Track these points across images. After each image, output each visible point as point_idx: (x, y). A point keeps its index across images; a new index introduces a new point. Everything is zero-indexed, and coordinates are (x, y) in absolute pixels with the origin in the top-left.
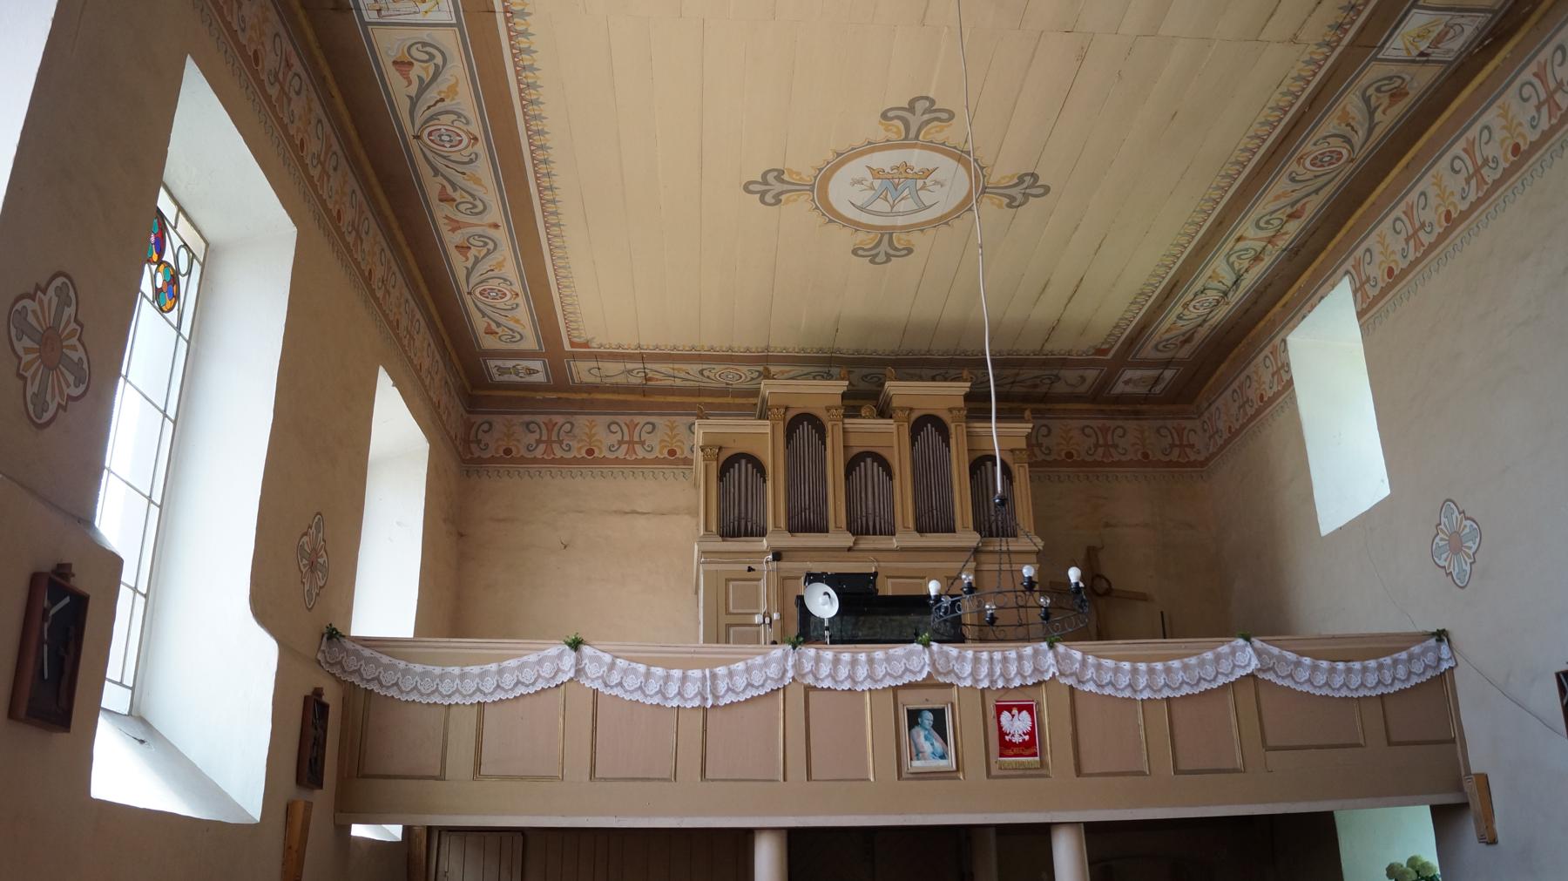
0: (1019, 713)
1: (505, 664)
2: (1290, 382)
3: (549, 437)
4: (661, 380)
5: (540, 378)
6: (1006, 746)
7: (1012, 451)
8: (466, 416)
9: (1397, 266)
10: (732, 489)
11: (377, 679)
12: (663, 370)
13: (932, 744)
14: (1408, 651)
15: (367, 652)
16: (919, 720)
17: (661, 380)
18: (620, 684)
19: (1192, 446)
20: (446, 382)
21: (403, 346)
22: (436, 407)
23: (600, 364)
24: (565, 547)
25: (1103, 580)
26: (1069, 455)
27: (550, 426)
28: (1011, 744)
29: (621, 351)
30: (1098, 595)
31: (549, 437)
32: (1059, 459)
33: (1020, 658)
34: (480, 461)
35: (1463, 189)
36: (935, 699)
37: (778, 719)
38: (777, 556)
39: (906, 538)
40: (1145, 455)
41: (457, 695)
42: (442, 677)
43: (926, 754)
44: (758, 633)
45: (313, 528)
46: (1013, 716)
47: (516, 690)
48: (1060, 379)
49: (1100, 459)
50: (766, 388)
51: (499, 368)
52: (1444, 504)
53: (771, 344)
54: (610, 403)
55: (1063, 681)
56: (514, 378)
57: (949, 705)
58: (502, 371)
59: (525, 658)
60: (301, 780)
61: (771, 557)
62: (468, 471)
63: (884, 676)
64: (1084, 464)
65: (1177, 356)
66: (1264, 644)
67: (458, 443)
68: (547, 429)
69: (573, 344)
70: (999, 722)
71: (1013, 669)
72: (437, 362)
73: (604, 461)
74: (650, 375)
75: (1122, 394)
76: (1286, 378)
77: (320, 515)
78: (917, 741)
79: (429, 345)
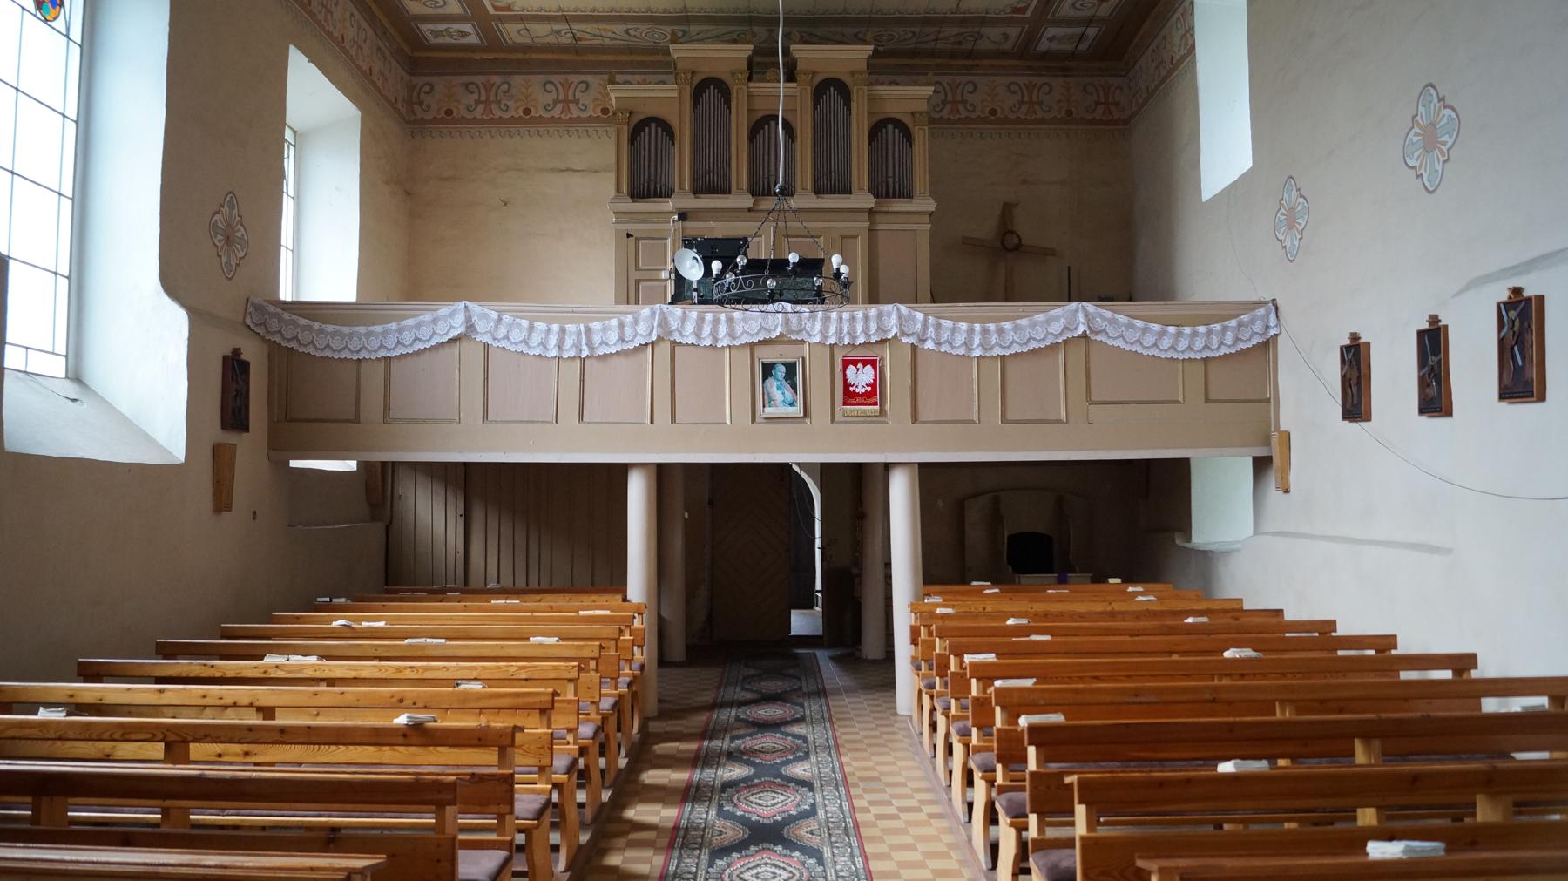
0: (864, 367)
1: (404, 323)
2: (1193, 47)
3: (488, 97)
4: (590, 40)
5: (473, 39)
6: (850, 395)
7: (913, 114)
8: (407, 77)
10: (643, 152)
11: (296, 338)
12: (589, 30)
13: (783, 393)
14: (1238, 319)
15: (286, 316)
16: (773, 372)
17: (590, 40)
18: (507, 338)
19: (1117, 104)
20: (379, 49)
21: (319, 22)
22: (368, 75)
23: (527, 26)
24: (506, 204)
25: (1014, 236)
26: (993, 112)
27: (488, 87)
28: (855, 394)
29: (543, 13)
30: (1010, 251)
31: (488, 97)
32: (983, 116)
33: (866, 318)
34: (423, 122)
36: (789, 354)
37: (645, 369)
38: (683, 216)
39: (804, 199)
40: (1070, 113)
41: (364, 351)
42: (351, 336)
43: (778, 403)
44: (665, 287)
45: (226, 206)
46: (858, 370)
47: (415, 345)
48: (982, 37)
49: (1023, 117)
50: (678, 52)
51: (432, 32)
53: (688, 6)
54: (545, 63)
55: (904, 340)
56: (448, 40)
57: (800, 360)
58: (437, 34)
59: (421, 317)
60: (226, 425)
61: (676, 217)
62: (412, 132)
63: (742, 334)
64: (1006, 121)
65: (1098, 14)
66: (1098, 309)
67: (399, 105)
68: (486, 90)
69: (496, 8)
70: (845, 375)
71: (859, 327)
72: (364, 29)
73: (540, 120)
74: (578, 35)
75: (1048, 51)
76: (1190, 42)
77: (233, 193)
78: (770, 390)
79: (352, 15)
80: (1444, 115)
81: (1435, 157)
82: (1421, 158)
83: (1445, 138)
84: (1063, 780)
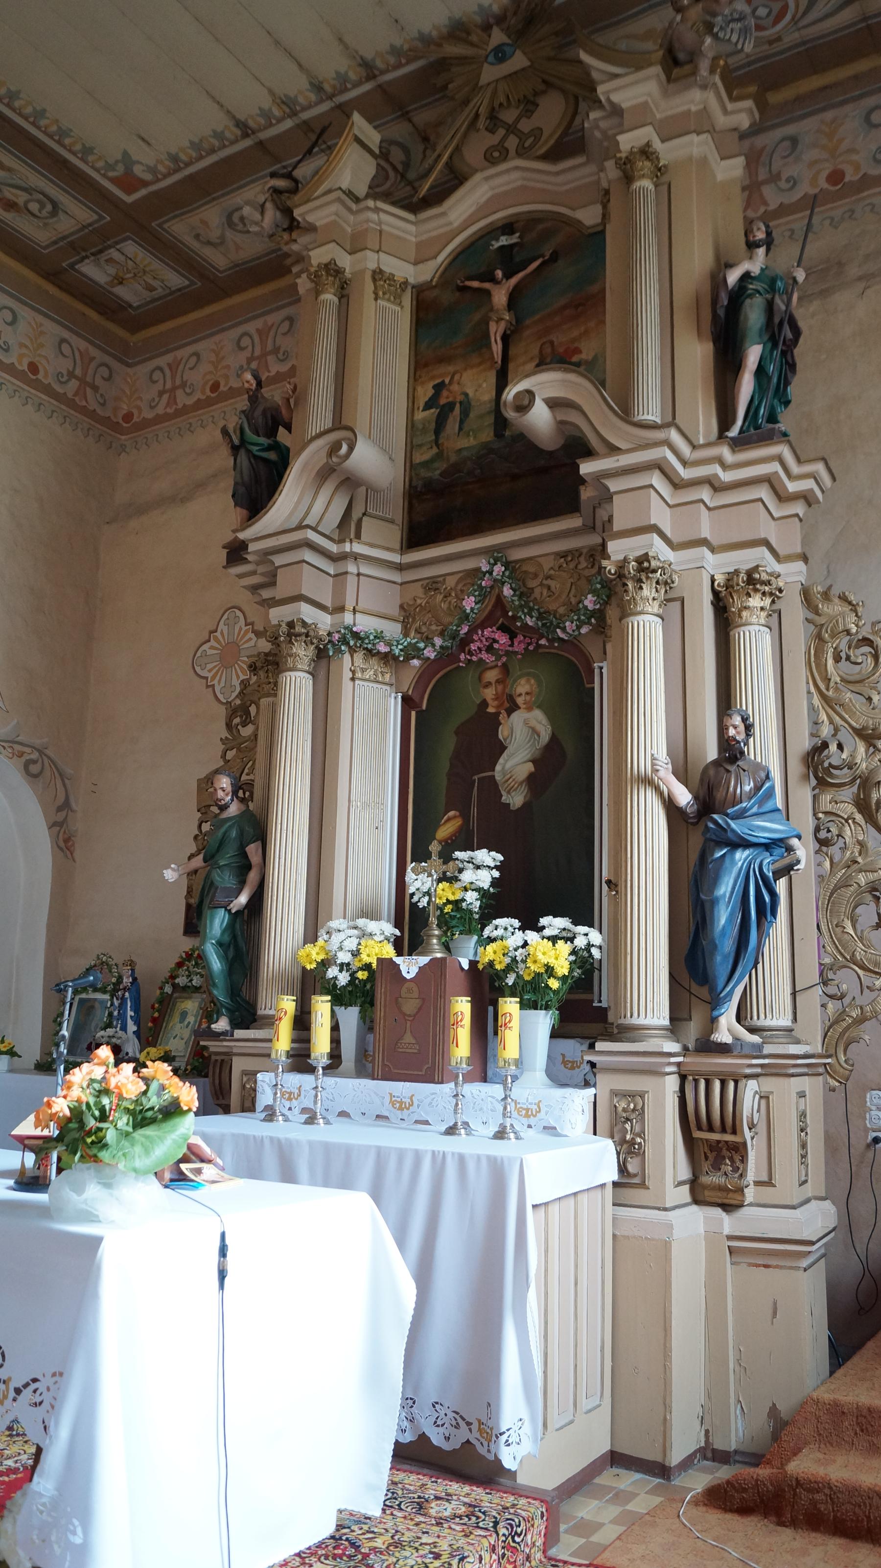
9: (140, 413)
35: (154, 399)
52: (230, 608)
80: (210, 671)
81: (226, 637)
82: (215, 671)
83: (210, 652)
84: (578, 468)
